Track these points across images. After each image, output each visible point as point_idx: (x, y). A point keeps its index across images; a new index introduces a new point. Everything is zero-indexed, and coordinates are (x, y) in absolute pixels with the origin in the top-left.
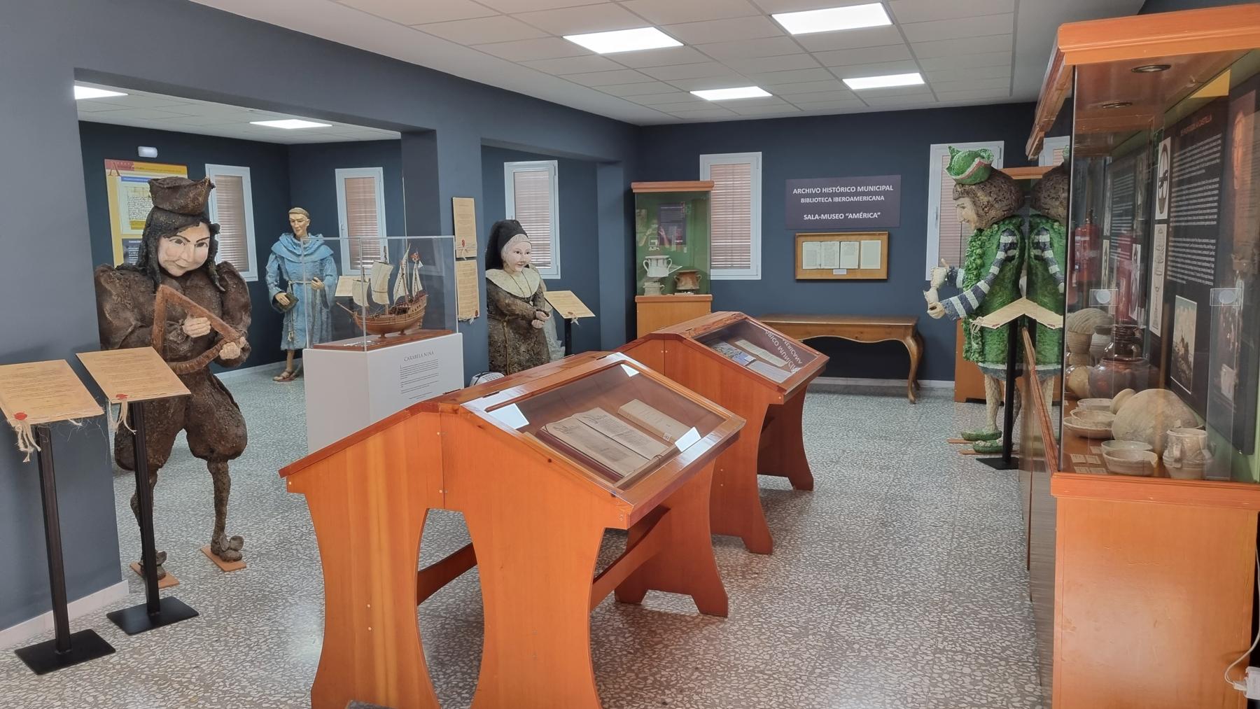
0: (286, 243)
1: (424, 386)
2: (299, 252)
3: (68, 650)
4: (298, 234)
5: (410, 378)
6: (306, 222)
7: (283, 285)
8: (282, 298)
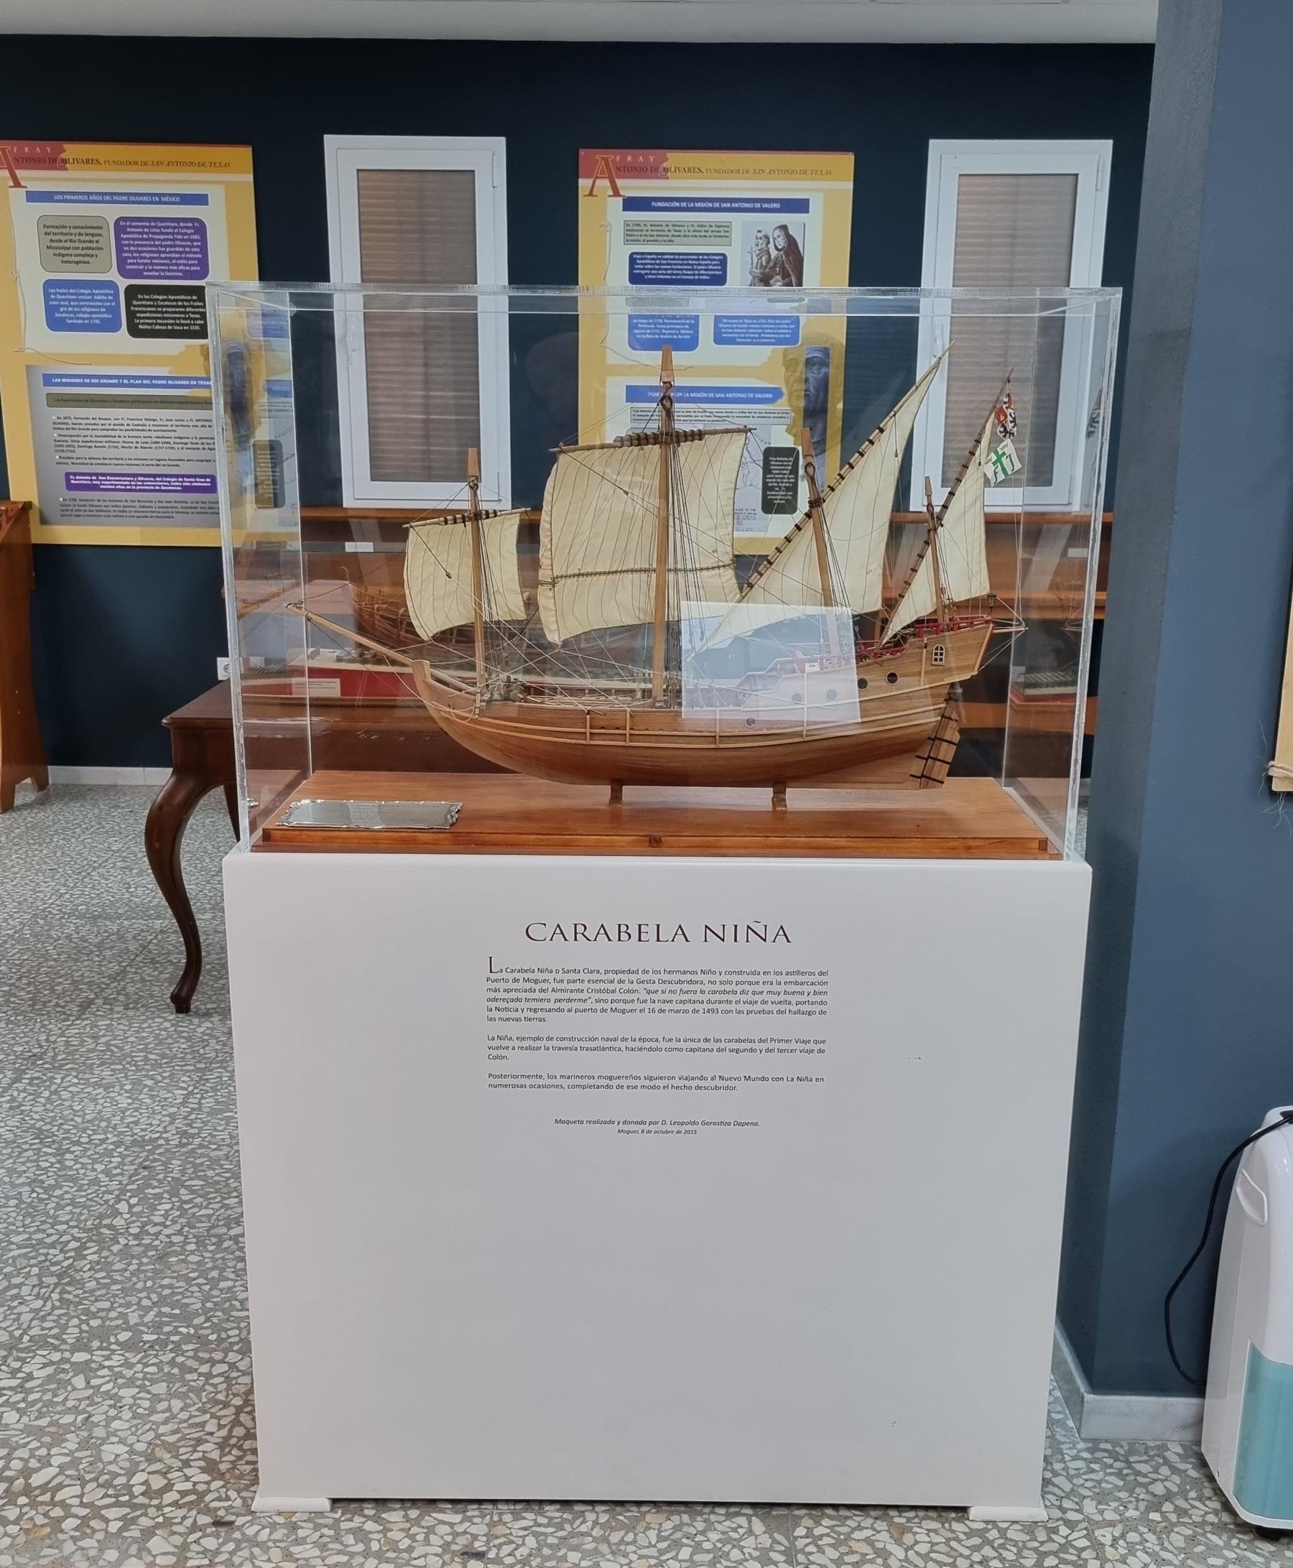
1: (725, 1083)
5: (559, 1025)
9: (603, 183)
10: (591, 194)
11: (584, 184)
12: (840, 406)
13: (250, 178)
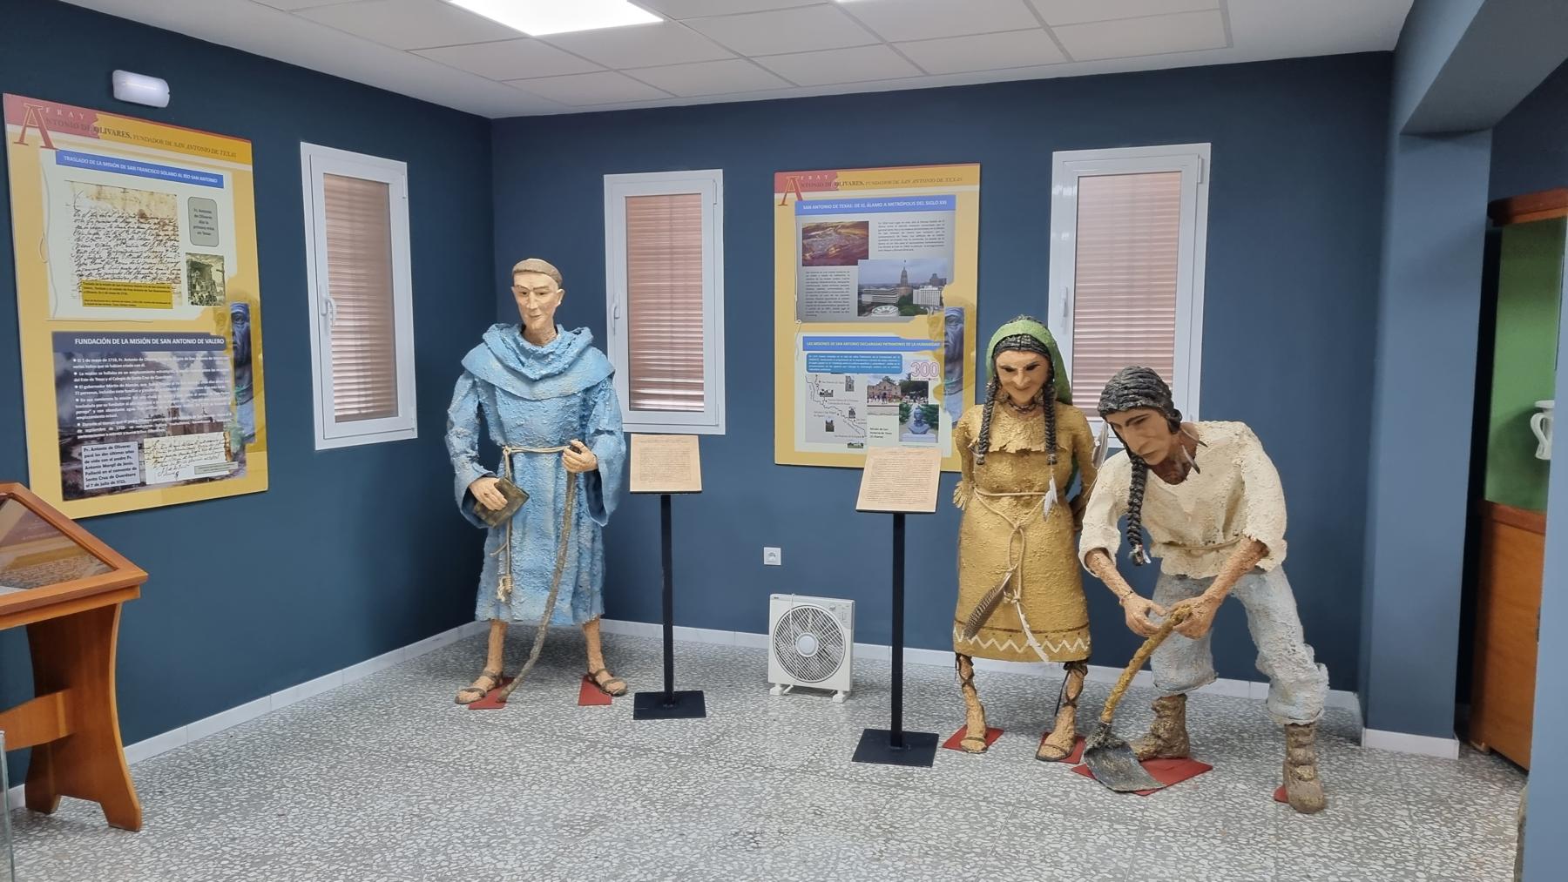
0: (500, 349)
2: (524, 377)
3: (897, 745)
4: (535, 325)
6: (555, 296)
7: (489, 455)
8: (487, 491)
9: (33, 133)
10: (21, 142)
11: (778, 197)
12: (261, 356)
13: (250, 168)
